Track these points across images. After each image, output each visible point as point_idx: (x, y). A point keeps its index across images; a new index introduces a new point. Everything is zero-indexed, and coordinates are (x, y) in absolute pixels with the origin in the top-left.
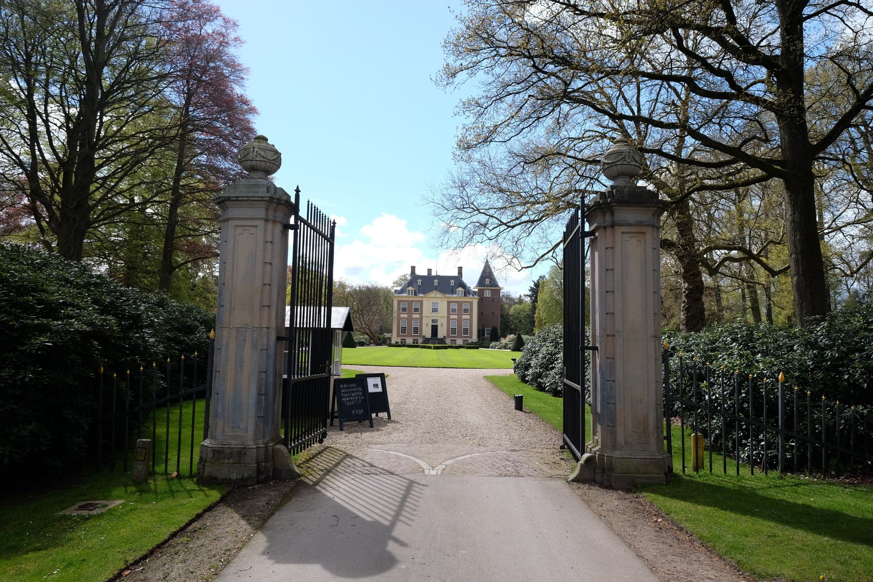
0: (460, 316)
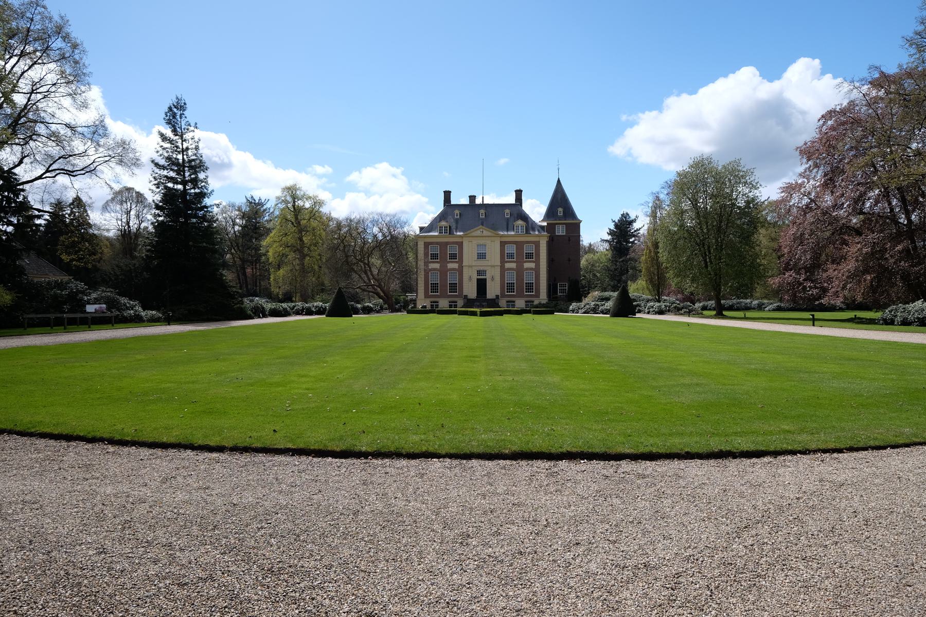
0: (520, 263)
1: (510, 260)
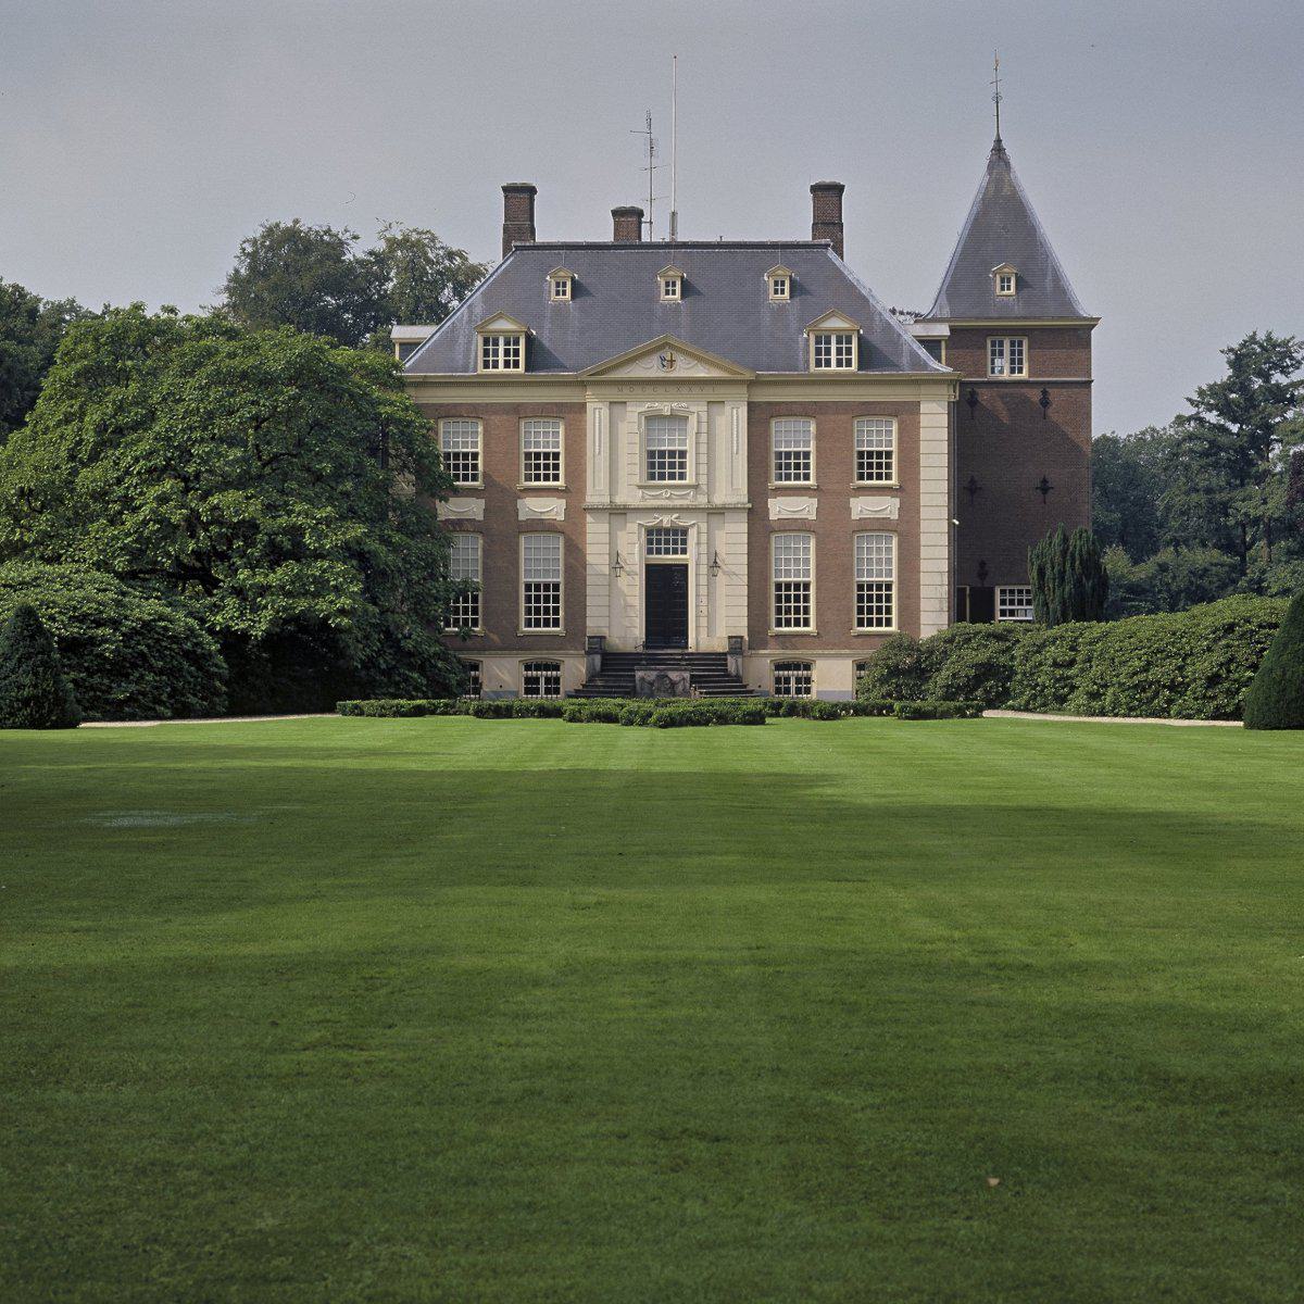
0: (832, 497)
1: (542, 483)
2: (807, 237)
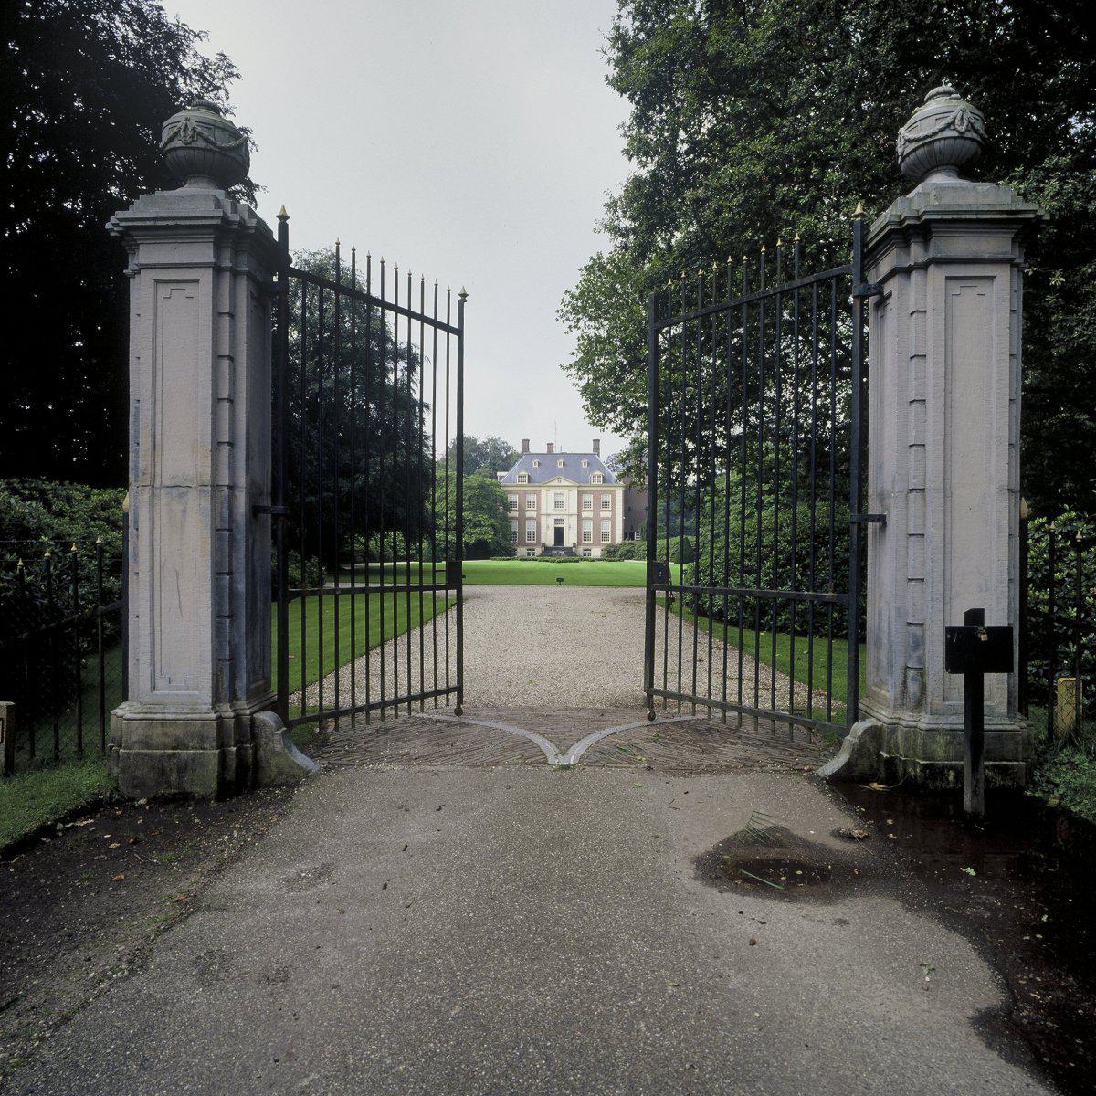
0: (596, 512)
2: (592, 452)
